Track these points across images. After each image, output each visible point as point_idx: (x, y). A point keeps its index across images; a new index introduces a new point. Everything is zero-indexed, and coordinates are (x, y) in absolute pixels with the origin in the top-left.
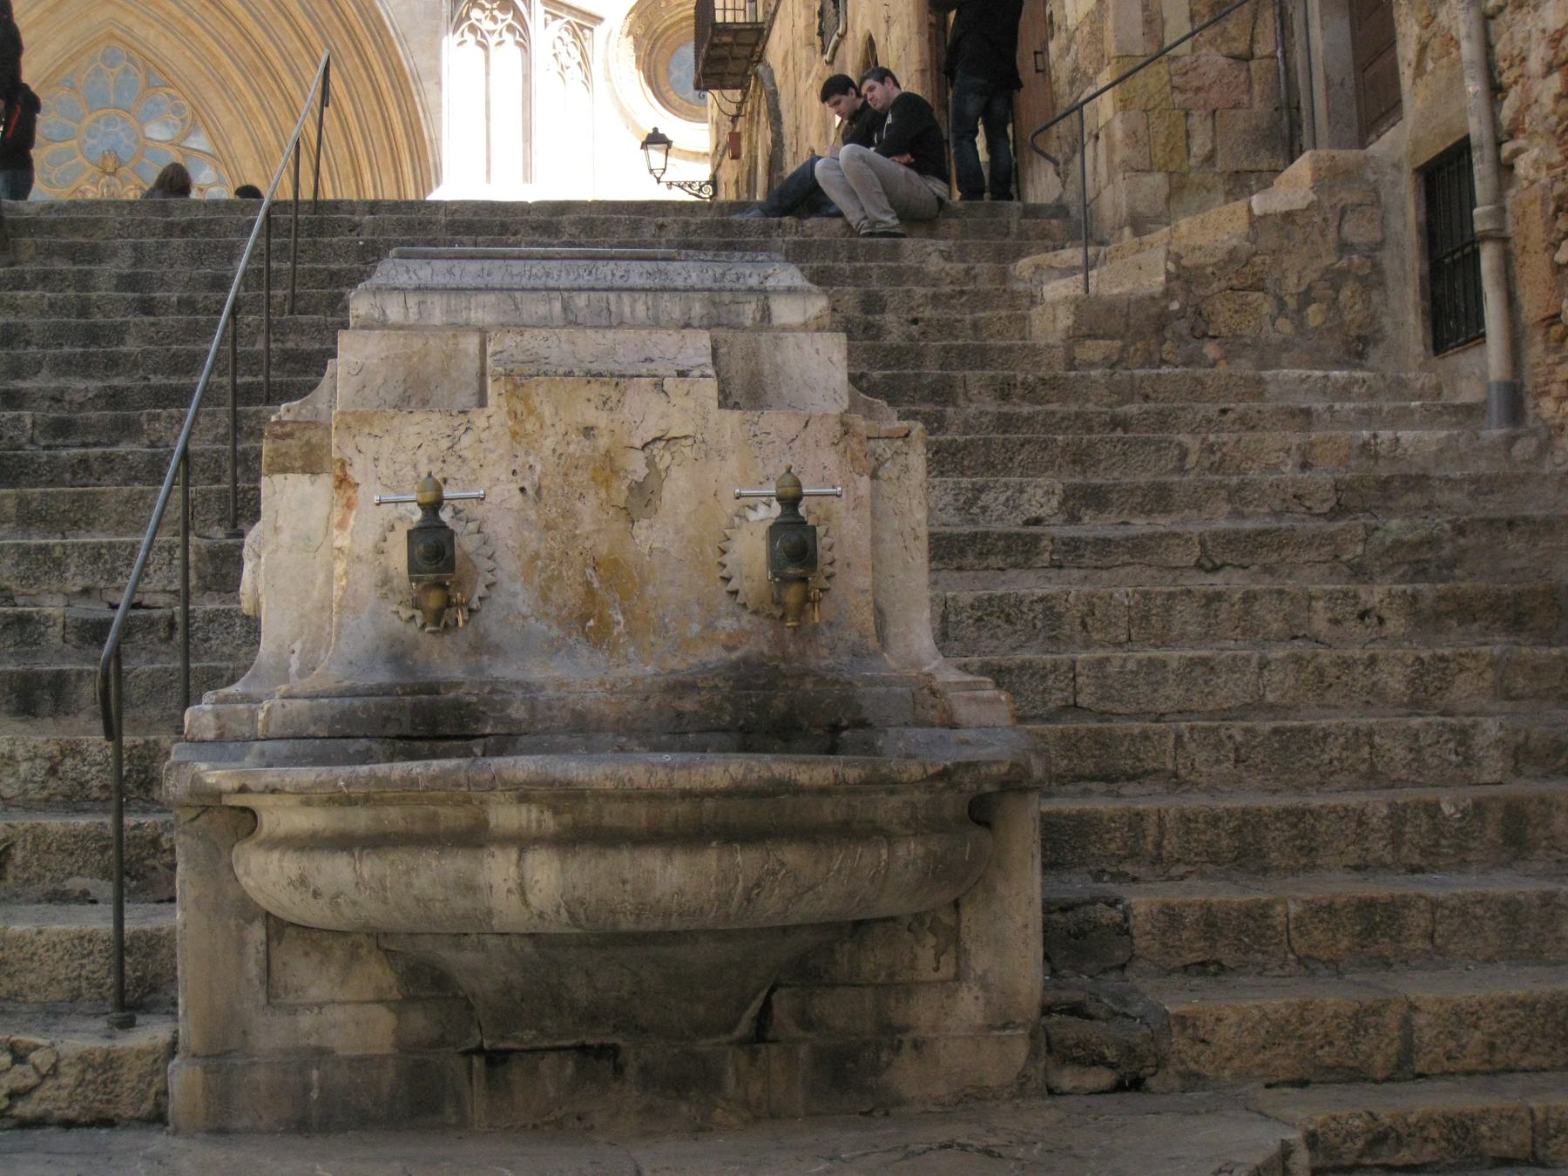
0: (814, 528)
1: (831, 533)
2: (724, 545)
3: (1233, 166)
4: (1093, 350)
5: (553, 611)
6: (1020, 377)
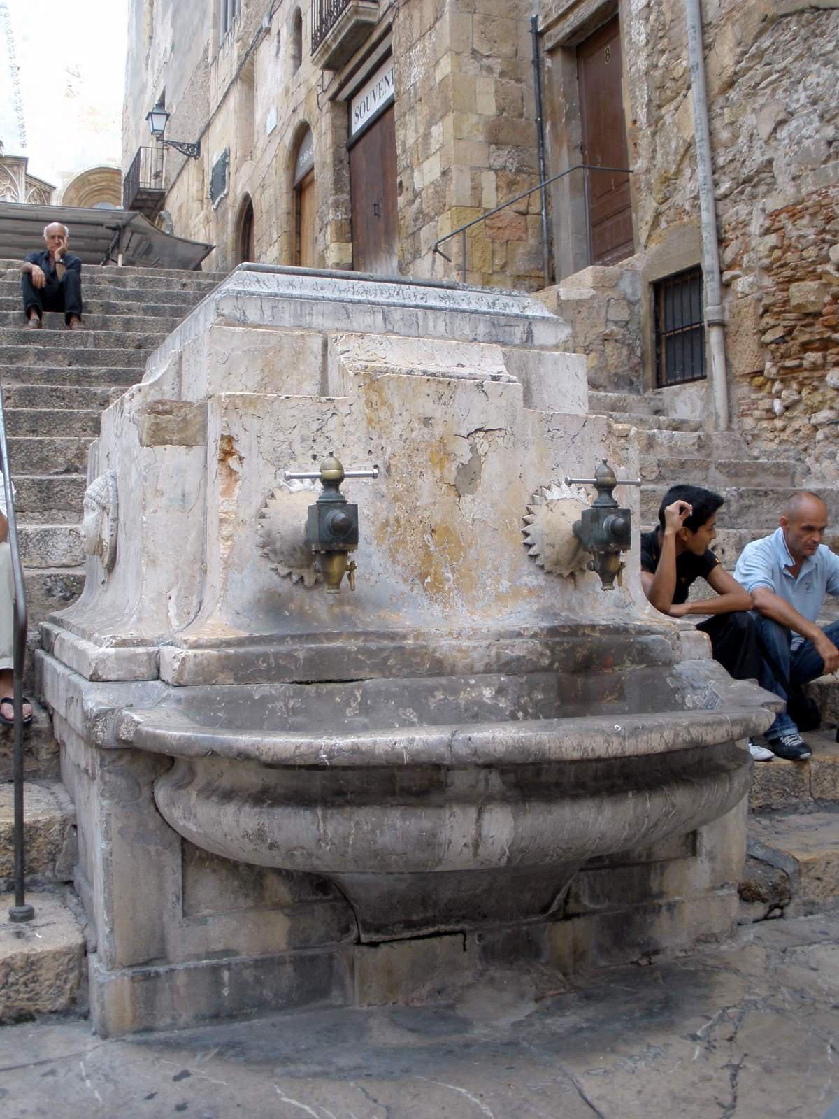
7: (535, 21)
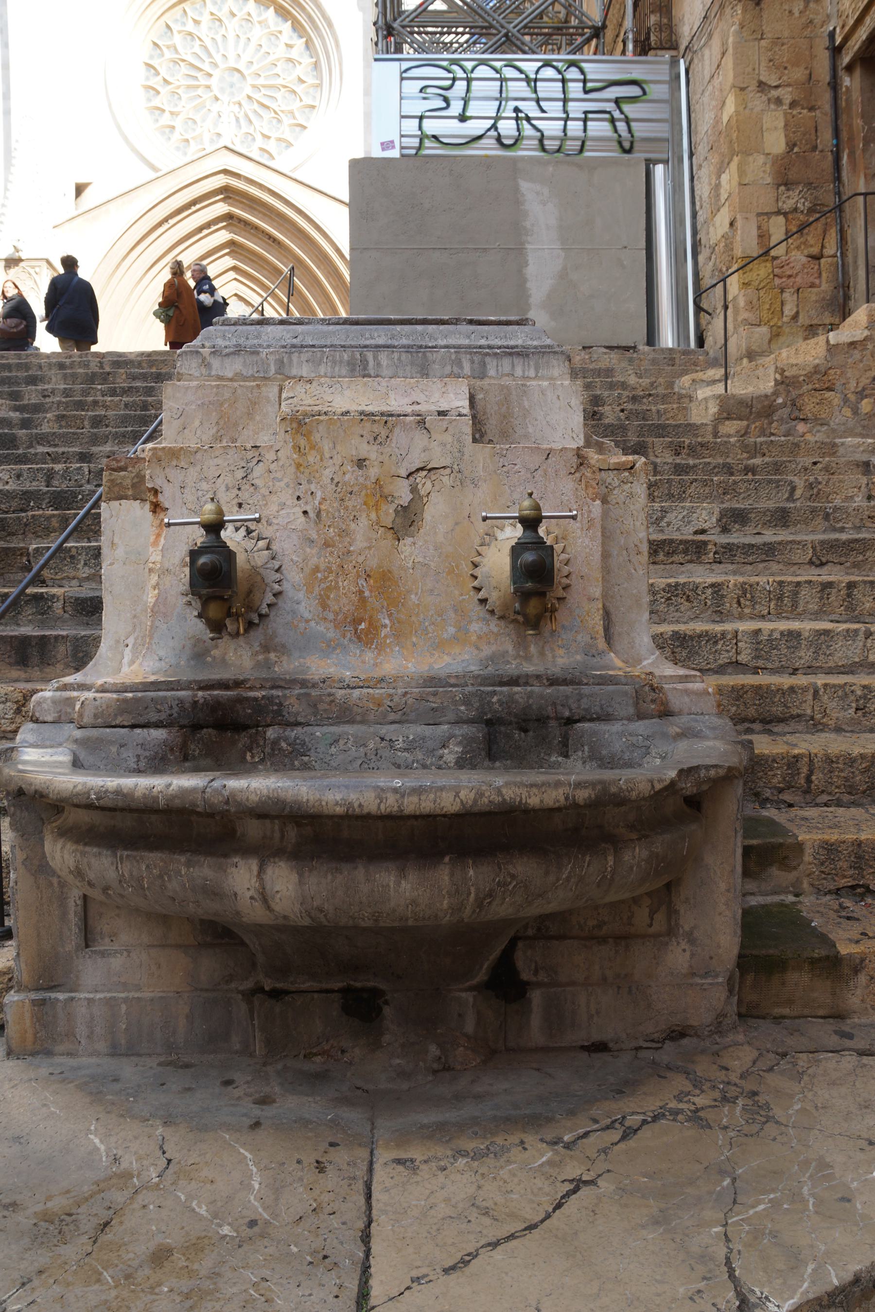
0: (552, 547)
1: (568, 549)
2: (477, 559)
3: (808, 322)
4: (731, 428)
5: (331, 616)
6: (687, 442)
7: (832, 35)
